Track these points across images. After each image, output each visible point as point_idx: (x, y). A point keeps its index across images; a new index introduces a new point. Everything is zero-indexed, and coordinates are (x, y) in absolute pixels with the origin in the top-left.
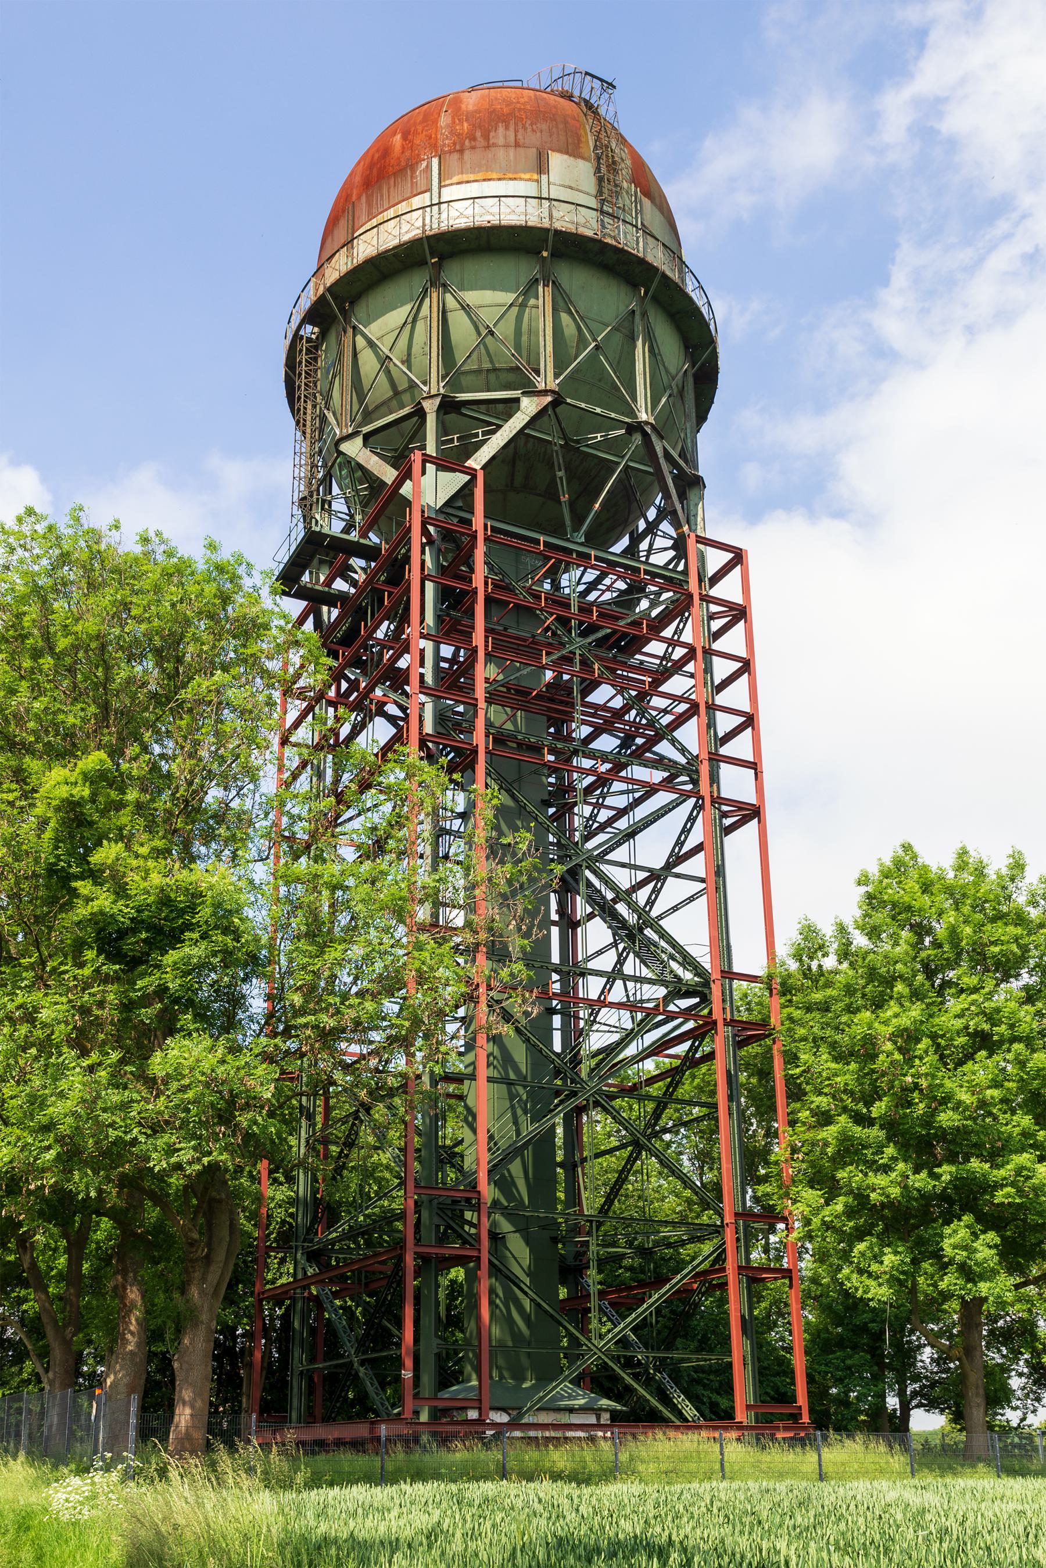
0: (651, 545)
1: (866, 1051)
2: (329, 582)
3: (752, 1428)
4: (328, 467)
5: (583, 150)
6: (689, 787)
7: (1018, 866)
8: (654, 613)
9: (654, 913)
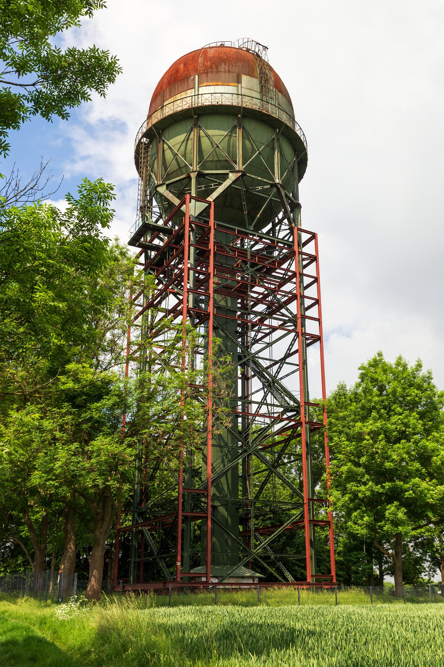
0: (280, 227)
1: (359, 437)
3: (313, 584)
7: (419, 366)
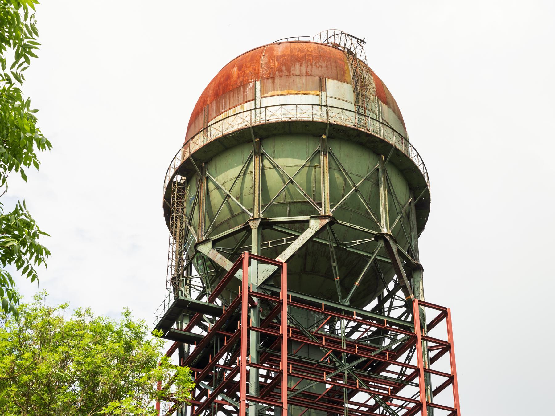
0: (391, 304)
4: (187, 258)
8: (394, 347)
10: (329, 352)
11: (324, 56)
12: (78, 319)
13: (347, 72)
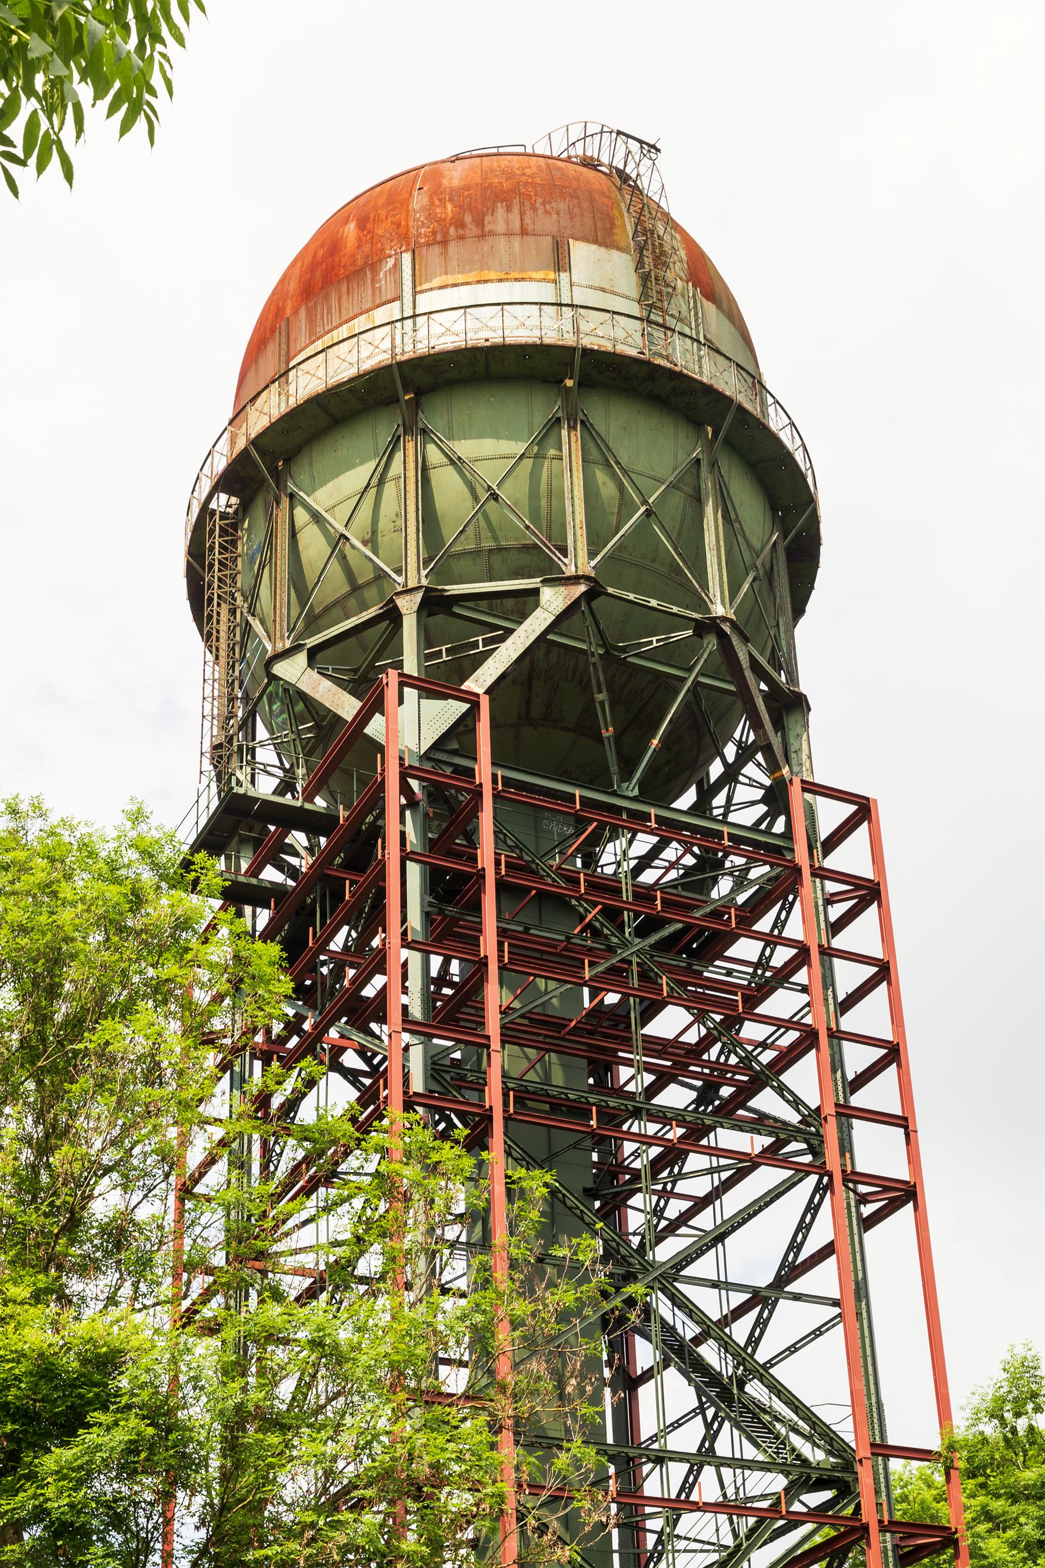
0: (729, 798)
2: (255, 870)
4: (250, 695)
5: (618, 238)
6: (807, 1159)
8: (741, 899)
9: (762, 1355)
10: (594, 912)
11: (563, 187)
12: (12, 825)
13: (618, 223)
